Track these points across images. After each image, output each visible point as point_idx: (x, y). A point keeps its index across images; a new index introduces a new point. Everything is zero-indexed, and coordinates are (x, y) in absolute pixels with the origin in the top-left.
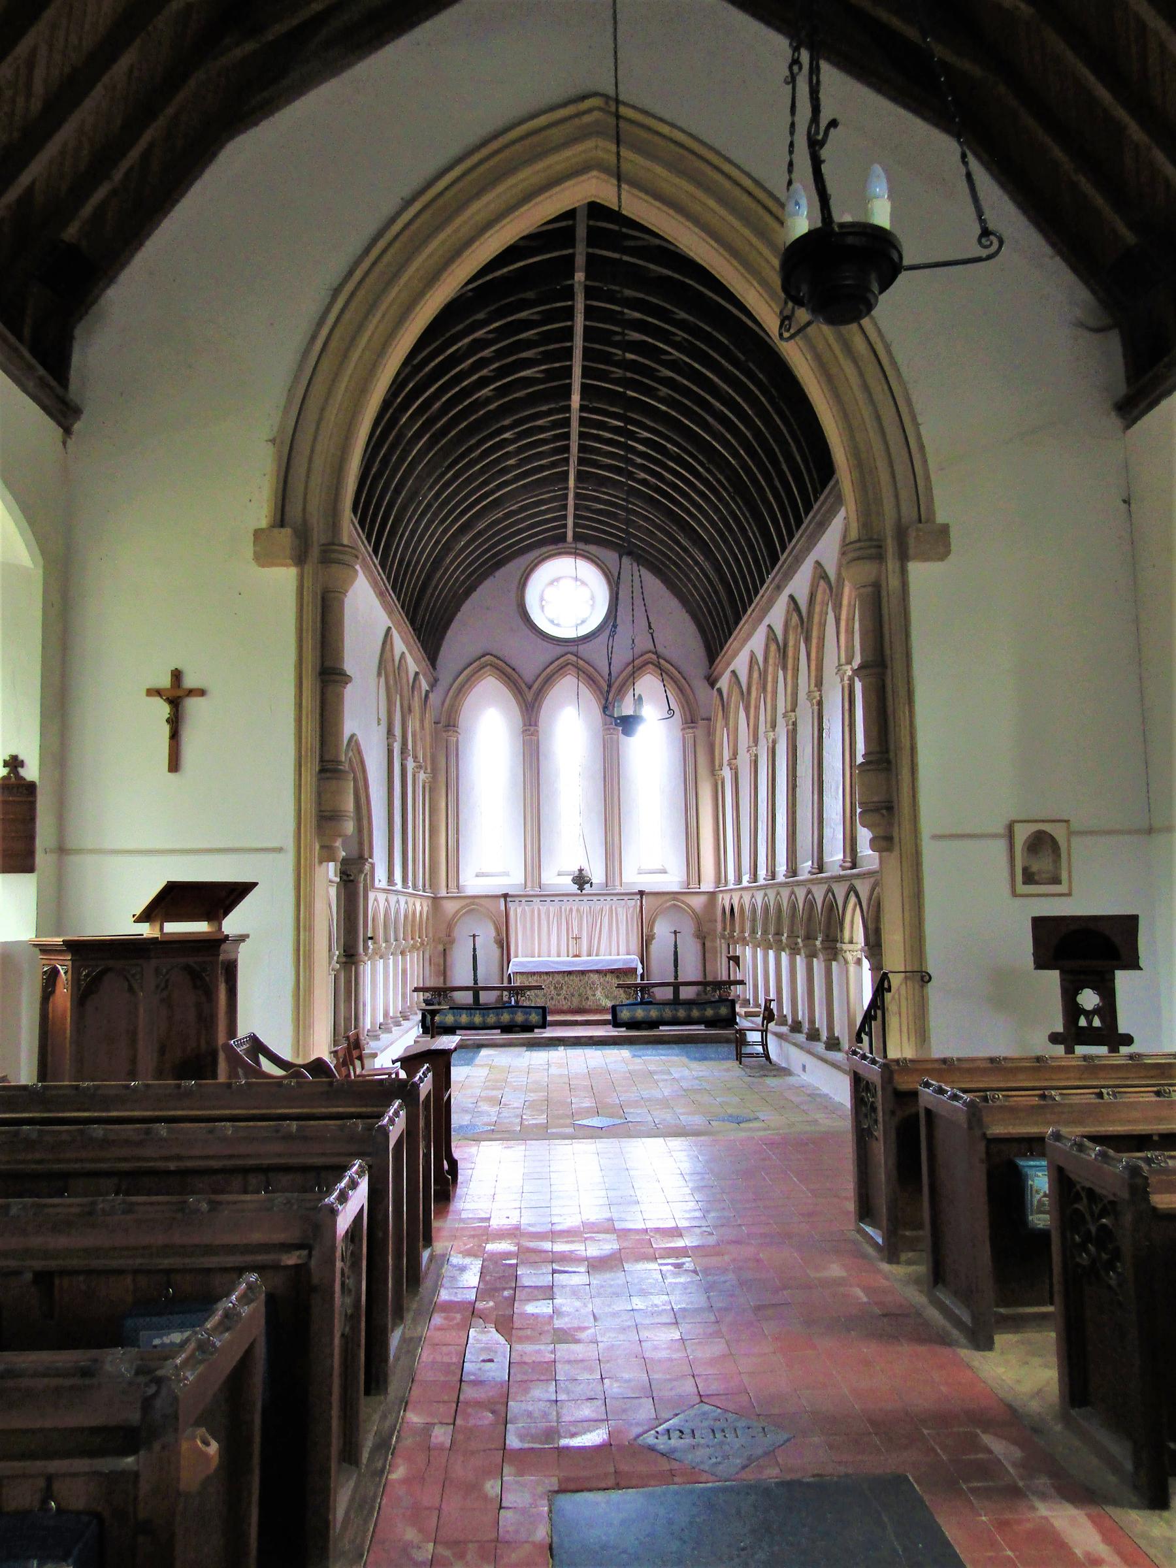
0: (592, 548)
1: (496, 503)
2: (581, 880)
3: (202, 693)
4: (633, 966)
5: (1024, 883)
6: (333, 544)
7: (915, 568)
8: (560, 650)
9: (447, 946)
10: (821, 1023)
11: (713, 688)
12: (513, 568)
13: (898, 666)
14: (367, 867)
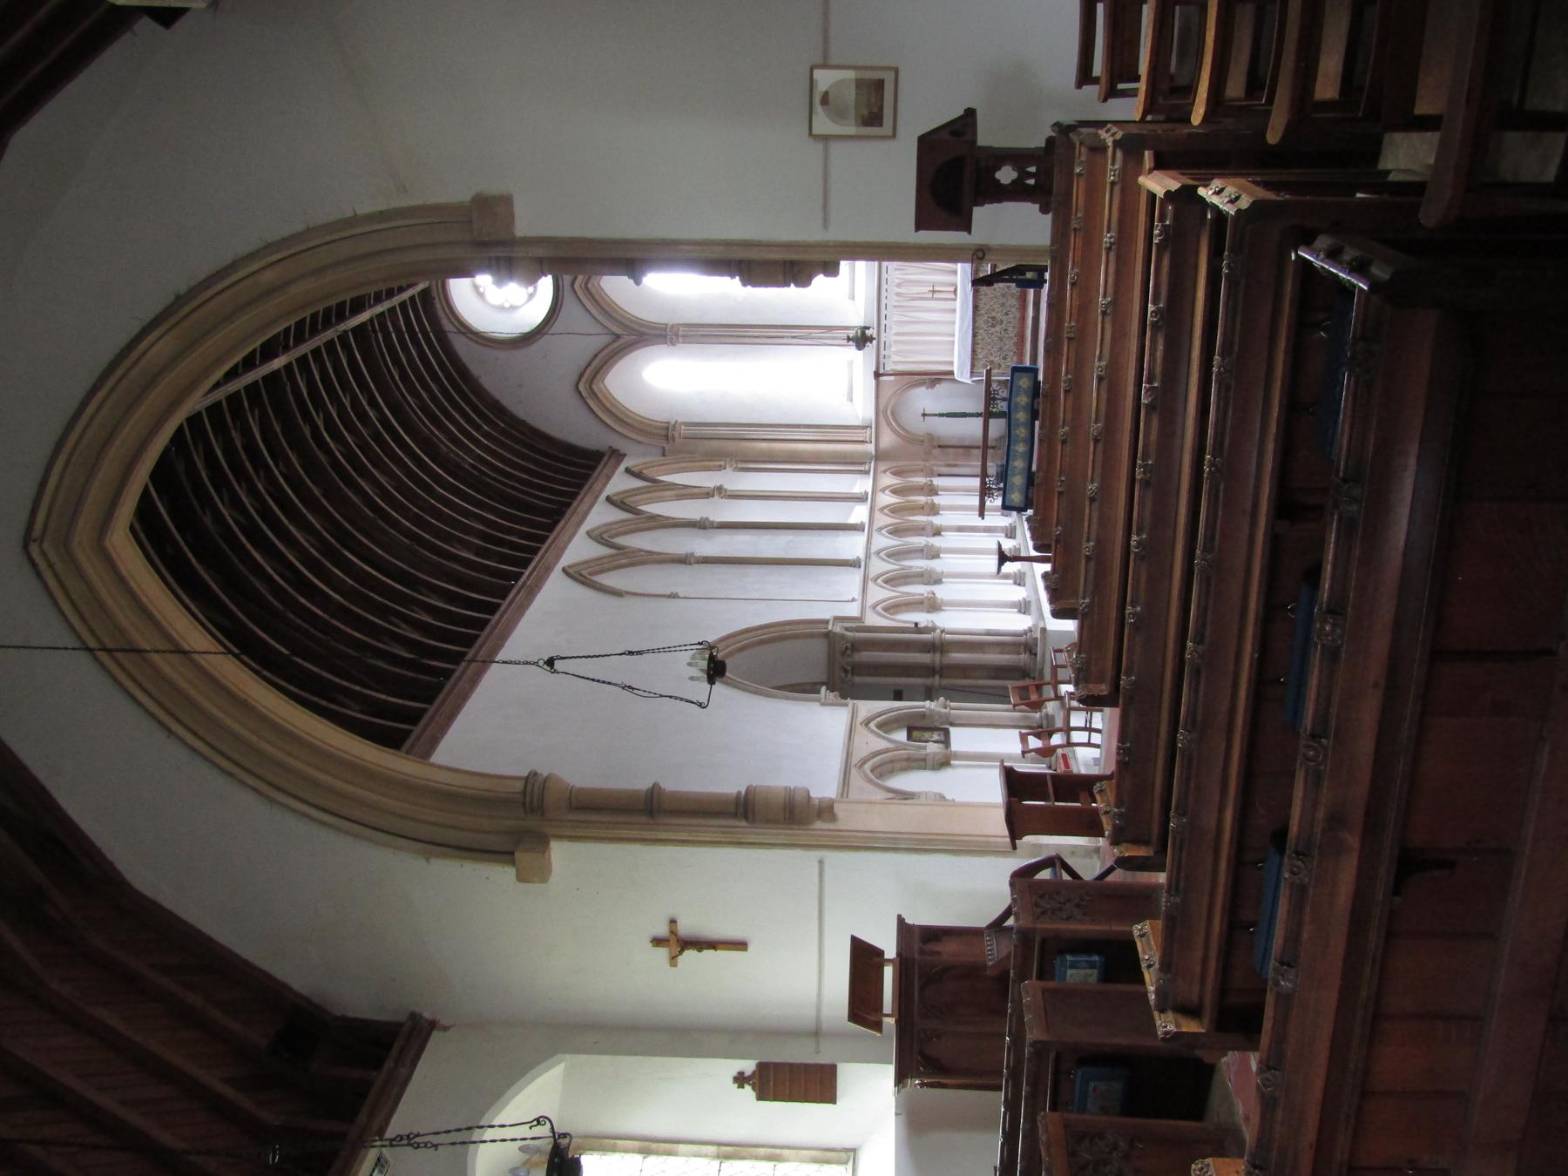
3: (673, 922)
5: (881, 125)
6: (524, 804)
9: (936, 443)
12: (460, 344)
14: (838, 629)
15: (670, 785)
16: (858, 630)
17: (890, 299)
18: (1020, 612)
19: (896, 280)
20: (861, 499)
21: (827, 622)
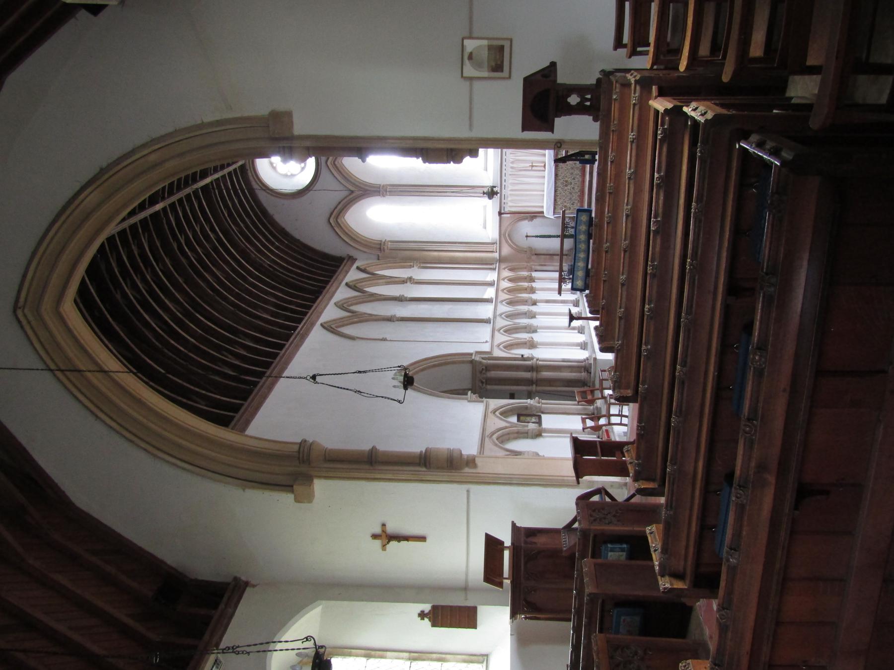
3: (384, 525)
5: (502, 71)
6: (299, 458)
9: (533, 253)
12: (262, 196)
14: (478, 358)
15: (382, 447)
16: (489, 359)
17: (508, 171)
18: (581, 348)
19: (511, 160)
20: (491, 284)
21: (471, 354)
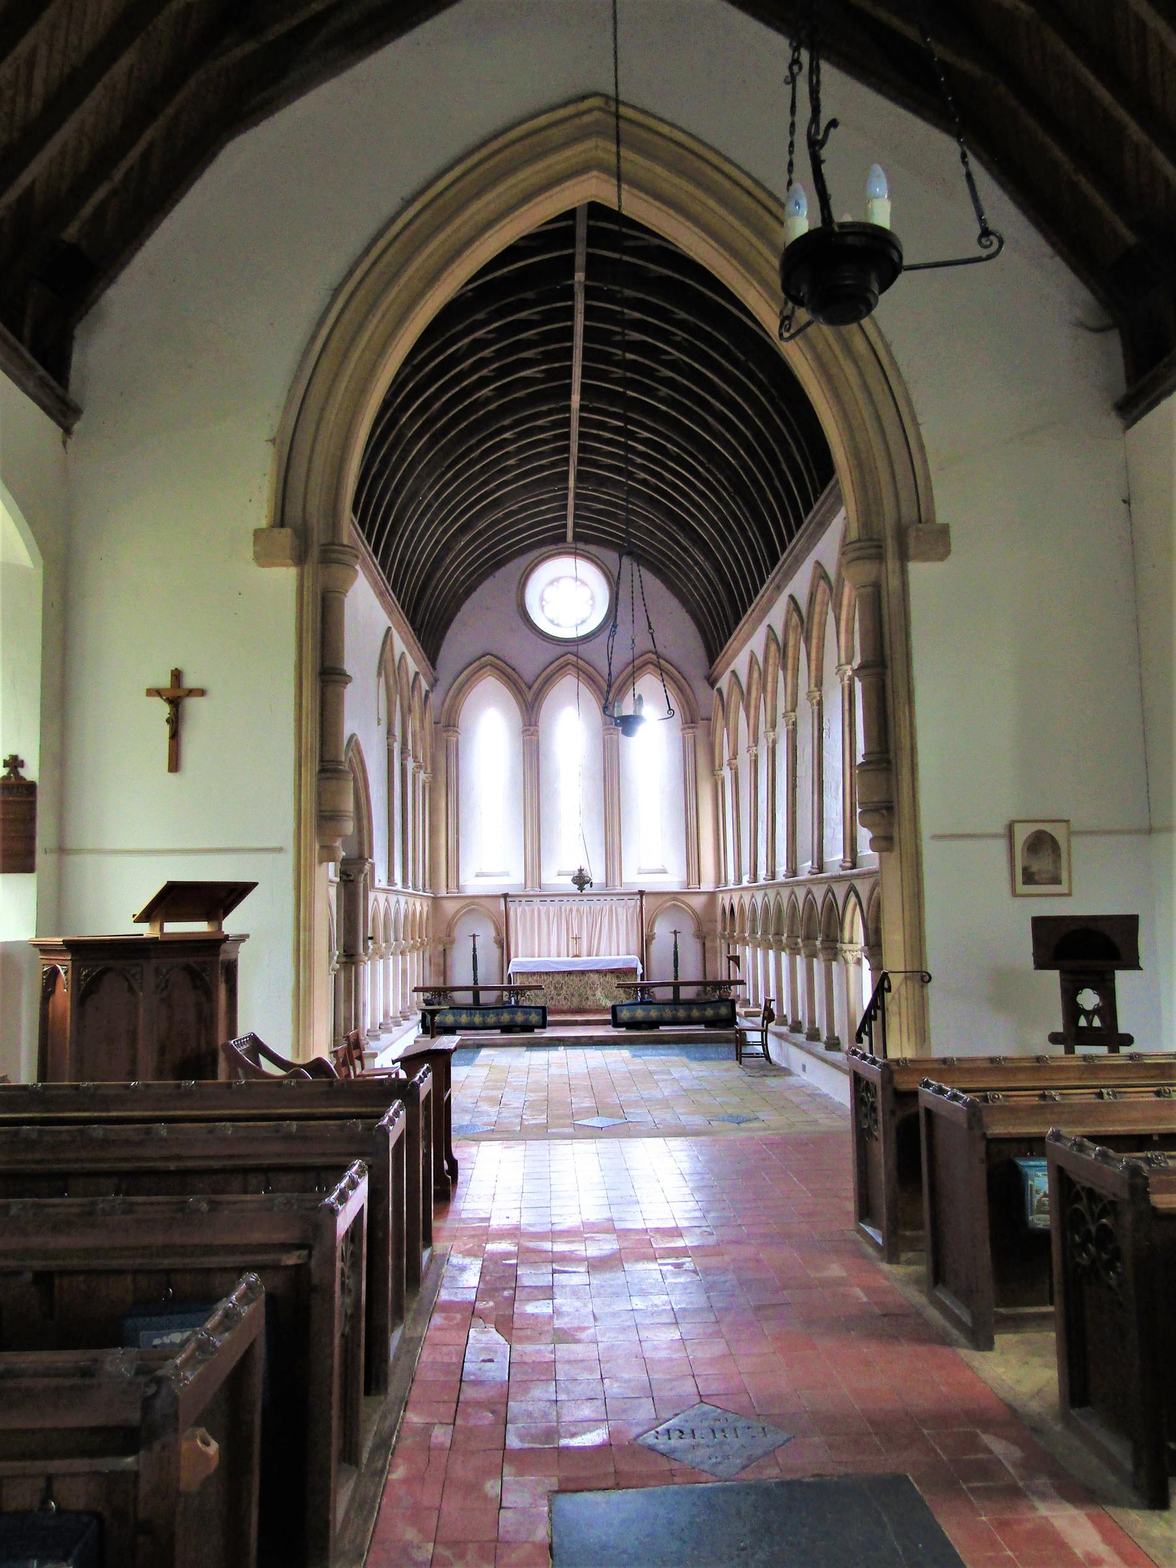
0: (592, 548)
1: (496, 503)
2: (581, 880)
3: (202, 693)
4: (633, 966)
5: (1024, 883)
6: (333, 544)
7: (915, 568)
8: (560, 650)
9: (447, 946)
10: (821, 1023)
11: (713, 688)
12: (513, 568)
13: (898, 666)
14: (367, 867)
